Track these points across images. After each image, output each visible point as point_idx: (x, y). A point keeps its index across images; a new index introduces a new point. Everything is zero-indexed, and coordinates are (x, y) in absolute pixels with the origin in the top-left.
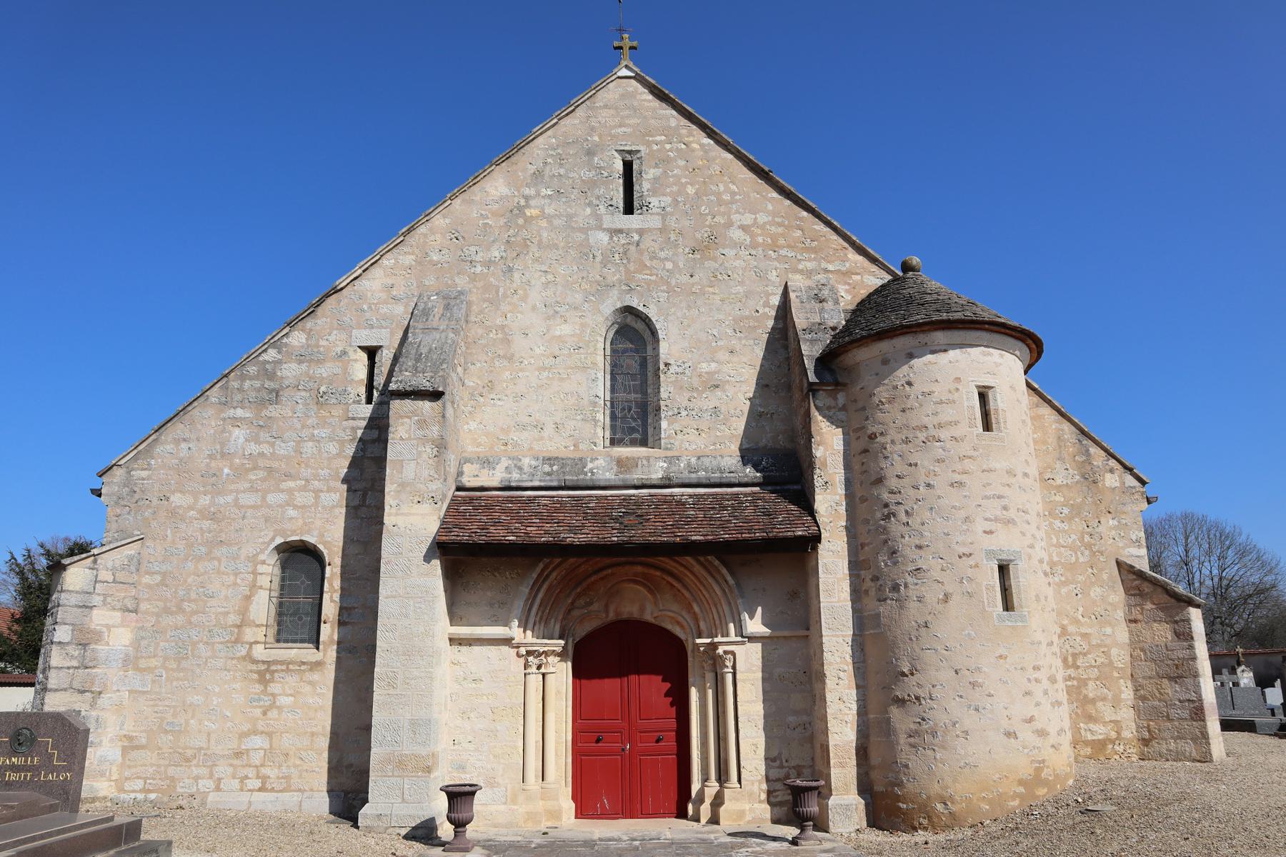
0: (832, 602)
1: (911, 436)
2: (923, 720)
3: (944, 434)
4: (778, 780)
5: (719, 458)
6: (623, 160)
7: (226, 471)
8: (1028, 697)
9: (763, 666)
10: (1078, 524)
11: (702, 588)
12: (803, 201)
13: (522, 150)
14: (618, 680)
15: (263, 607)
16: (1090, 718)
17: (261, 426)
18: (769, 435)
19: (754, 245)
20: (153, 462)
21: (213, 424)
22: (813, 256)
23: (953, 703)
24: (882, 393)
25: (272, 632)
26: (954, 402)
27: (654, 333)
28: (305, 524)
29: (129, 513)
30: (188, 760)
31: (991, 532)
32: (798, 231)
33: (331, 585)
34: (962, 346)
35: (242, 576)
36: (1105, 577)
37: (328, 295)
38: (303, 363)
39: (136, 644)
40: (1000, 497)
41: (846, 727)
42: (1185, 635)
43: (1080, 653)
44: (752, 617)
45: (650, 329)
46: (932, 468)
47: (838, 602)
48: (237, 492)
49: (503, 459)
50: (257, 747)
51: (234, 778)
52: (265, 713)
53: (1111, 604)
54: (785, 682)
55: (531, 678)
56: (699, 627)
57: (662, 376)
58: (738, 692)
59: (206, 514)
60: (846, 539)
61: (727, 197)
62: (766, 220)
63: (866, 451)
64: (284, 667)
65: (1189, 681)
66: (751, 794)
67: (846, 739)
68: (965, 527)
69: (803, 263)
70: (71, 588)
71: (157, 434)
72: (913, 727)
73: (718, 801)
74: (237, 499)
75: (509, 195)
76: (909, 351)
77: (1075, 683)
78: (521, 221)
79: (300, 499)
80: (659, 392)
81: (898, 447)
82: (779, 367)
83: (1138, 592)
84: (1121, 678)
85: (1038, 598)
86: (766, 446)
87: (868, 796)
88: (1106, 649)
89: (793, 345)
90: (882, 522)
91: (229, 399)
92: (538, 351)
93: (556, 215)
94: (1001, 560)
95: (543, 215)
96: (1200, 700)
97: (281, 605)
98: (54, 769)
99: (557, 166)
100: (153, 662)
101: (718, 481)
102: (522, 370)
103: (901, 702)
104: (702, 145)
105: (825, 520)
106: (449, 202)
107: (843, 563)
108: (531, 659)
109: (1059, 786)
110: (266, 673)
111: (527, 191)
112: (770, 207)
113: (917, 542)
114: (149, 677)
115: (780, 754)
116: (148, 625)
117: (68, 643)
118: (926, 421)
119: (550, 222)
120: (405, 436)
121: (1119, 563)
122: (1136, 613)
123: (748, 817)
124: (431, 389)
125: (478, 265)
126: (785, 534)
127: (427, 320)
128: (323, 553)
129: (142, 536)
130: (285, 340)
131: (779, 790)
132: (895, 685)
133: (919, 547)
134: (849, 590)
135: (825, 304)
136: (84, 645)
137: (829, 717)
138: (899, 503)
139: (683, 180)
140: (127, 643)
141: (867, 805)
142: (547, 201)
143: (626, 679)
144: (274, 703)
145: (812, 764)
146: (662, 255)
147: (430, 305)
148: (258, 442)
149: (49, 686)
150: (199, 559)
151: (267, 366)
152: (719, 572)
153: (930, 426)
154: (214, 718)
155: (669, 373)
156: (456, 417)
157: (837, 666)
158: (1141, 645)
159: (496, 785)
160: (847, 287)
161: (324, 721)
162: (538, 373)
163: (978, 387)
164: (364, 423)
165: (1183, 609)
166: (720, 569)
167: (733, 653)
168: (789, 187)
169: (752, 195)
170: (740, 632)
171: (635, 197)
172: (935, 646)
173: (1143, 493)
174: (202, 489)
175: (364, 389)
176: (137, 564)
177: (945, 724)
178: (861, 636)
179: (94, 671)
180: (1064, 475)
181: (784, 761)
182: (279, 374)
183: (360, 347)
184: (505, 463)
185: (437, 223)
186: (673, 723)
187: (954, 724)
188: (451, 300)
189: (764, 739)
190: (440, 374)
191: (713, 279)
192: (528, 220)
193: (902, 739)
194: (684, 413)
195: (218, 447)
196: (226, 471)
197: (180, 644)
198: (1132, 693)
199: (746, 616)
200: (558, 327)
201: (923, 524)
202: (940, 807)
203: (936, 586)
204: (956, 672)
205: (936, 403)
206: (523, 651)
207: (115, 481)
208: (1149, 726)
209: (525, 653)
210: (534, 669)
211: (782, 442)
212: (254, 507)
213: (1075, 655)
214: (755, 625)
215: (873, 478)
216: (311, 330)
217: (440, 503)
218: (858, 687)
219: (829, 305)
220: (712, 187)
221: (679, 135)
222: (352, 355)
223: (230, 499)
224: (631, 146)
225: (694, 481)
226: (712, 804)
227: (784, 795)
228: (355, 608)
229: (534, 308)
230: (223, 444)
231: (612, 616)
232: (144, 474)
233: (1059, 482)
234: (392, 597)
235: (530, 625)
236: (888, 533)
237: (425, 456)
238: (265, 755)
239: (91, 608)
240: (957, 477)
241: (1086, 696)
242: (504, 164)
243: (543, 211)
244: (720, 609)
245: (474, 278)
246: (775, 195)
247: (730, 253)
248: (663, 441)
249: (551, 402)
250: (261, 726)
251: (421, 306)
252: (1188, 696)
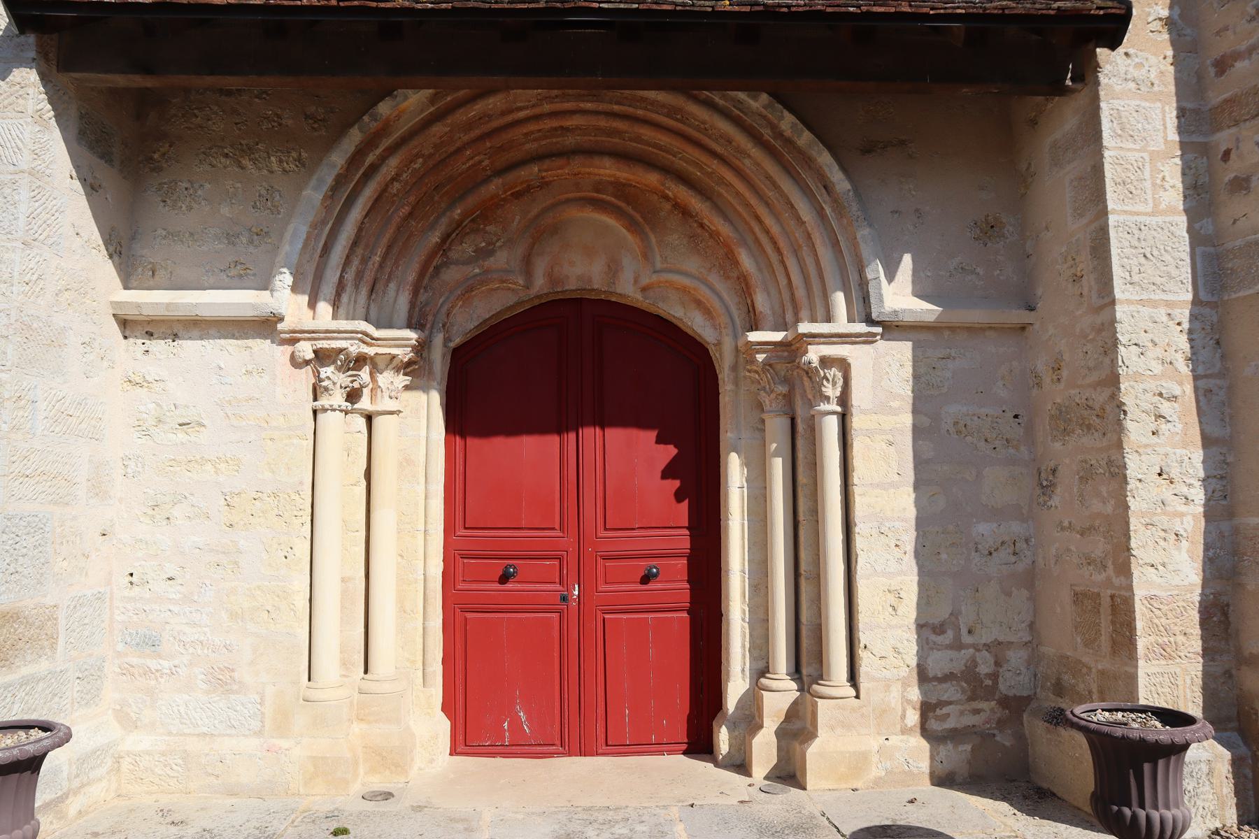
0: (1138, 214)
4: (948, 677)
9: (915, 398)
11: (762, 211)
14: (554, 440)
41: (1179, 549)
44: (891, 277)
47: (1152, 214)
54: (969, 439)
55: (330, 421)
60: (1170, 53)
67: (1176, 581)
73: (797, 725)
87: (1235, 736)
107: (1163, 112)
108: (327, 371)
115: (955, 614)
131: (950, 703)
134: (1180, 186)
143: (572, 436)
145: (1029, 638)
152: (808, 161)
157: (1152, 385)
159: (235, 687)
166: (814, 153)
167: (843, 365)
170: (863, 308)
178: (1213, 305)
181: (964, 631)
186: (683, 541)
189: (916, 578)
206: (306, 350)
209: (310, 355)
210: (338, 399)
226: (781, 733)
227: (962, 713)
231: (540, 284)
235: (329, 288)
244: (809, 261)
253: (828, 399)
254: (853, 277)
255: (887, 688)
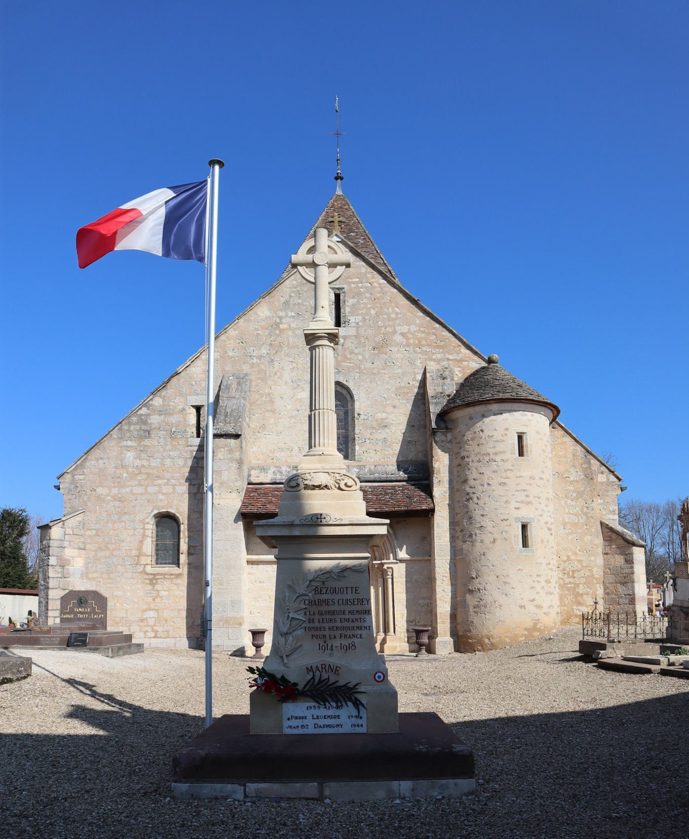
1: (481, 458)
2: (481, 600)
3: (498, 458)
5: (386, 466)
6: (335, 293)
7: (125, 475)
8: (532, 589)
10: (581, 502)
12: (437, 318)
13: (277, 289)
15: (149, 546)
16: (579, 604)
17: (142, 451)
18: (413, 453)
19: (408, 345)
20: (85, 470)
21: (116, 450)
22: (441, 351)
23: (495, 592)
24: (469, 435)
25: (154, 559)
26: (504, 441)
27: (352, 396)
28: (169, 502)
29: (75, 498)
30: (117, 623)
31: (518, 508)
32: (433, 336)
33: (184, 534)
34: (510, 411)
35: (138, 530)
36: (593, 530)
37: (172, 377)
38: (162, 415)
39: (86, 565)
40: (524, 490)
42: (630, 561)
43: (577, 570)
44: (401, 550)
45: (350, 394)
46: (491, 475)
48: (132, 486)
49: (272, 467)
50: (151, 616)
51: (141, 632)
52: (154, 600)
53: (595, 545)
56: (375, 555)
57: (356, 421)
58: (394, 588)
59: (116, 498)
61: (393, 316)
62: (415, 329)
63: (460, 465)
64: (162, 577)
65: (630, 584)
66: (400, 638)
68: (505, 506)
69: (435, 355)
70: (54, 538)
71: (86, 455)
72: (476, 603)
73: (383, 643)
74: (132, 490)
75: (271, 316)
76: (482, 413)
77: (573, 585)
78: (277, 332)
79: (165, 489)
80: (354, 430)
81: (475, 464)
82: (420, 415)
83: (609, 538)
84: (597, 583)
85: (542, 541)
86: (411, 460)
88: (590, 568)
89: (427, 405)
90: (466, 503)
91: (123, 436)
92: (289, 407)
93: (297, 328)
94: (523, 522)
95: (290, 328)
96: (634, 594)
97: (157, 545)
98: (96, 613)
99: (297, 298)
100: (96, 575)
101: (385, 479)
102: (281, 418)
103: (471, 592)
104: (380, 284)
105: (438, 500)
106: (237, 321)
109: (546, 632)
110: (153, 580)
111: (281, 314)
112: (418, 322)
113: (482, 513)
114: (94, 583)
115: (415, 619)
116: (91, 556)
117: (55, 566)
118: (489, 450)
119: (294, 332)
120: (222, 458)
121: (601, 523)
122: (608, 550)
123: (398, 650)
124: (234, 433)
125: (255, 358)
126: (416, 508)
127: (229, 392)
128: (179, 518)
129: (84, 511)
130: (151, 402)
132: (469, 583)
133: (483, 515)
135: (446, 380)
136: (63, 566)
137: (437, 599)
138: (474, 493)
139: (369, 306)
140: (82, 566)
141: (454, 642)
142: (292, 319)
144: (158, 595)
146: (357, 351)
147: (229, 383)
148: (141, 459)
149: (50, 587)
150: (115, 522)
151: (142, 417)
153: (491, 454)
154: (128, 602)
155: (360, 419)
156: (246, 445)
158: (609, 566)
160: (460, 369)
161: (183, 603)
162: (289, 420)
163: (517, 433)
164: (196, 448)
165: (630, 547)
168: (429, 310)
169: (407, 314)
170: (395, 558)
171: (341, 316)
172: (488, 564)
173: (619, 485)
174: (113, 485)
175: (195, 429)
176: (83, 524)
177: (491, 601)
178: (455, 559)
179: (69, 579)
180: (576, 475)
181: (417, 622)
182: (149, 421)
183: (192, 406)
184: (272, 469)
185: (231, 333)
187: (495, 602)
188: (241, 379)
190: (239, 424)
191: (385, 365)
192: (282, 331)
193: (471, 609)
194: (368, 441)
195: (120, 462)
196: (125, 475)
197: (108, 565)
198: (603, 591)
199: (398, 550)
200: (300, 394)
201: (485, 504)
202: (486, 640)
203: (489, 535)
204: (497, 577)
205: (495, 441)
207: (66, 481)
208: (609, 607)
211: (421, 457)
212: (141, 494)
213: (573, 571)
214: (403, 554)
215: (463, 480)
216: (165, 396)
217: (241, 493)
218: (452, 585)
219: (448, 381)
220: (385, 310)
221: (367, 278)
222: (188, 411)
223: (128, 490)
224: (339, 285)
225: (372, 479)
228: (197, 546)
229: (286, 383)
230: (122, 460)
232: (81, 477)
233: (572, 479)
234: (219, 540)
236: (468, 508)
237: (232, 468)
238: (155, 620)
239: (64, 548)
240: (503, 480)
241: (578, 593)
242: (267, 297)
243: (289, 326)
245: (252, 365)
246: (421, 314)
247: (394, 349)
248: (356, 457)
249: (297, 436)
250: (152, 606)
251: (224, 383)
252: (628, 593)
253: (389, 575)
254: (394, 550)
255: (401, 633)
